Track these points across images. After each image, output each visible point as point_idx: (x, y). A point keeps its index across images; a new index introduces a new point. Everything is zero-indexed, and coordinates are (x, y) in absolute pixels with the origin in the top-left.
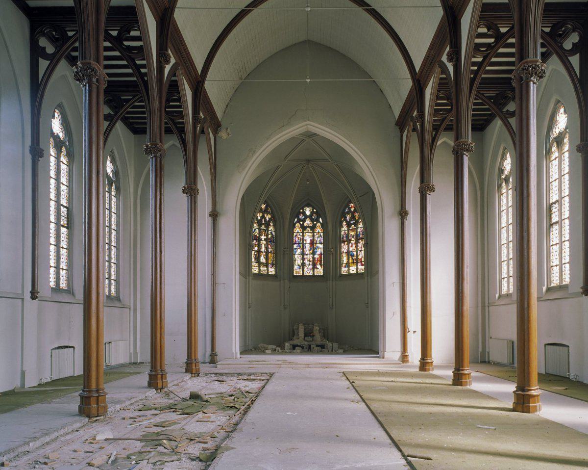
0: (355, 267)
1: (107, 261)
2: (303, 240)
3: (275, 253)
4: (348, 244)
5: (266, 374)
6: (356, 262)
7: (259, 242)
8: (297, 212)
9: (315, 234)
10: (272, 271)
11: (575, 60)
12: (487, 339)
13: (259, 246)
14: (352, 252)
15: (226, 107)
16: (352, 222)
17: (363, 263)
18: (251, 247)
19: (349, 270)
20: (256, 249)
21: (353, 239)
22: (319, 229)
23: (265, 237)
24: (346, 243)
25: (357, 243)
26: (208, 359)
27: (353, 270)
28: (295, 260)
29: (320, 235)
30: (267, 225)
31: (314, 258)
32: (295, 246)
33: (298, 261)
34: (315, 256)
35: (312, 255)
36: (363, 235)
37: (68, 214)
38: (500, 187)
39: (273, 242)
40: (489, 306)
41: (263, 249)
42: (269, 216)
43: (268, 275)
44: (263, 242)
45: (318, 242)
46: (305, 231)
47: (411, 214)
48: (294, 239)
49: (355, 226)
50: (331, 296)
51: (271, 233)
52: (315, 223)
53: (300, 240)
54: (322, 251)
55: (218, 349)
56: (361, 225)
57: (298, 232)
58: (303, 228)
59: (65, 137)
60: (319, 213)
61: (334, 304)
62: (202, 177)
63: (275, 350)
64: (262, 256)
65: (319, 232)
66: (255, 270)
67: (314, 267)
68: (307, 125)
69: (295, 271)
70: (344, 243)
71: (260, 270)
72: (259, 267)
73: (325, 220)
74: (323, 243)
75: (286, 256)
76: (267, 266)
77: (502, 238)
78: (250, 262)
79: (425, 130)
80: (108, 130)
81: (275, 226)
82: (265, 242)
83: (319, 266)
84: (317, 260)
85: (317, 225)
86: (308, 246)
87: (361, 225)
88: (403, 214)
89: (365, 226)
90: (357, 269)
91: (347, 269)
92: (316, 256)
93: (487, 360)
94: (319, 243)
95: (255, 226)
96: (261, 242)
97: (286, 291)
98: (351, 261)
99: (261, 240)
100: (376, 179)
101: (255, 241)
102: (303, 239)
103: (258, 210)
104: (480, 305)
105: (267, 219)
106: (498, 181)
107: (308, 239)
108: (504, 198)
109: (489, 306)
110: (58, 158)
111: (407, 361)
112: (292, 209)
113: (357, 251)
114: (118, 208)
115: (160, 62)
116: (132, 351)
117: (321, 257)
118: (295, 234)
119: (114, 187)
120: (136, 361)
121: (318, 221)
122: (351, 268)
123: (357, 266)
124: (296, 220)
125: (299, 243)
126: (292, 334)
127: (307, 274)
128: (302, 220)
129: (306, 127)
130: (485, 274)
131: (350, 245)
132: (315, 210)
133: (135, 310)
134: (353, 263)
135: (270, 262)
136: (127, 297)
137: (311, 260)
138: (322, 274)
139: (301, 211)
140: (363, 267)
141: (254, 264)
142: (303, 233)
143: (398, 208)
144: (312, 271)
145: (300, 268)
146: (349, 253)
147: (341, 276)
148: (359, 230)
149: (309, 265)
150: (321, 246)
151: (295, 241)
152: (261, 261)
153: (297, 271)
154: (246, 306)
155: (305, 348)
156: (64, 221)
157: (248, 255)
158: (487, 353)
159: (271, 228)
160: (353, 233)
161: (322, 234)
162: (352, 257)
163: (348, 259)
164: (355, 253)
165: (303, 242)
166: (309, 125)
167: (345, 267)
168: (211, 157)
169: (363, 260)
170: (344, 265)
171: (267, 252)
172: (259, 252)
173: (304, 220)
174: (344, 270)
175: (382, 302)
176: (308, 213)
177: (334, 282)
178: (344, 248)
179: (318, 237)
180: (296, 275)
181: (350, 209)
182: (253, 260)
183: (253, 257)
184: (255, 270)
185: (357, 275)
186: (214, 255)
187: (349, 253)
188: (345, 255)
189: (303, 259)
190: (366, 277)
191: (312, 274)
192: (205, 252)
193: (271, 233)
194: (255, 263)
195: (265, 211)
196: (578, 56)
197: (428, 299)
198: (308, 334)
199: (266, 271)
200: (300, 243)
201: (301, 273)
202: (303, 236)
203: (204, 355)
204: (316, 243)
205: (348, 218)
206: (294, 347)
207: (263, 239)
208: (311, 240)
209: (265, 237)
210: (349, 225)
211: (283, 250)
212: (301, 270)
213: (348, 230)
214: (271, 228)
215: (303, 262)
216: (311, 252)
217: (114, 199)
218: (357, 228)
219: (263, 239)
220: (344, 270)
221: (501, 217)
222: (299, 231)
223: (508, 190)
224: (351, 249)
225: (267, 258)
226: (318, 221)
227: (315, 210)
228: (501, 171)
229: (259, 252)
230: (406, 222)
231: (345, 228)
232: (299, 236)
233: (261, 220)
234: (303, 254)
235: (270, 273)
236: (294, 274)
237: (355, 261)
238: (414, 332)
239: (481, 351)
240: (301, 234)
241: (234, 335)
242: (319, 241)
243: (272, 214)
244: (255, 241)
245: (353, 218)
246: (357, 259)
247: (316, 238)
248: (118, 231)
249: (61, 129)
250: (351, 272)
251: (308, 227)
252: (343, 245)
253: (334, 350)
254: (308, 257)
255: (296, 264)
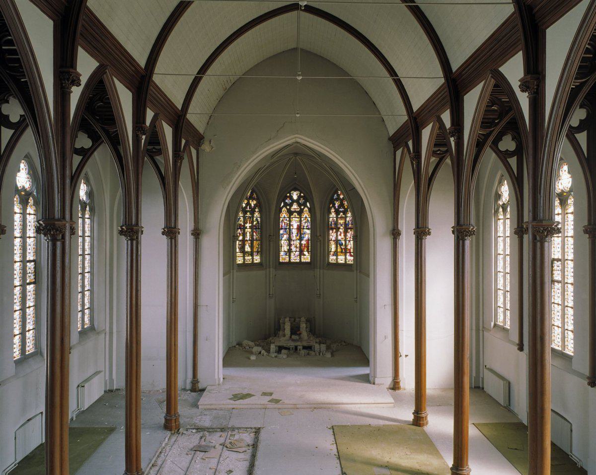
0: (344, 257)
1: (80, 236)
2: (290, 225)
3: (261, 240)
4: (337, 232)
5: (251, 428)
6: (345, 251)
7: (244, 231)
8: (283, 196)
9: (302, 219)
10: (257, 259)
11: (582, 138)
12: (481, 368)
13: (244, 234)
14: (340, 240)
15: (210, 118)
16: (341, 210)
17: (352, 254)
18: (235, 238)
19: (337, 259)
20: (241, 238)
21: (341, 228)
22: (306, 214)
23: (250, 225)
24: (334, 230)
25: (346, 232)
26: (189, 386)
27: (341, 259)
28: (281, 246)
29: (308, 220)
30: (252, 212)
31: (300, 244)
32: (281, 232)
33: (285, 248)
34: (302, 242)
35: (299, 241)
36: (352, 224)
37: (35, 268)
38: (497, 212)
39: (259, 229)
40: (483, 331)
41: (248, 237)
42: (255, 202)
43: (253, 264)
44: (248, 230)
45: (305, 228)
46: (292, 216)
47: (404, 233)
48: (281, 224)
49: (343, 214)
50: (318, 288)
51: (257, 219)
52: (302, 207)
53: (287, 225)
54: (310, 236)
55: (200, 376)
56: (349, 215)
57: (284, 217)
58: (290, 213)
59: (33, 185)
60: (306, 198)
61: (322, 293)
62: (182, 188)
63: (260, 353)
64: (247, 244)
65: (306, 217)
66: (240, 260)
67: (301, 253)
68: (295, 138)
69: (281, 257)
70: (333, 231)
71: (244, 259)
72: (244, 257)
73: (312, 204)
74: (311, 229)
75: (271, 243)
76: (252, 255)
77: (498, 265)
78: (234, 253)
79: (421, 175)
80: (79, 170)
81: (260, 212)
82: (250, 230)
83: (306, 253)
84: (304, 246)
85: (305, 210)
86: (294, 232)
87: (349, 215)
88: (395, 234)
89: (353, 215)
90: (346, 259)
91: (335, 257)
92: (304, 242)
93: (481, 386)
94: (307, 229)
95: (241, 214)
96: (246, 230)
97: (271, 279)
98: (339, 250)
99: (246, 228)
100: (368, 197)
101: (239, 230)
102: (290, 224)
103: (245, 197)
104: (474, 328)
105: (253, 205)
106: (495, 206)
107: (295, 224)
108: (500, 223)
109: (483, 331)
110: (24, 214)
111: (399, 388)
112: (279, 194)
113: (345, 241)
114: (92, 230)
115: (137, 136)
116: (107, 378)
117: (308, 243)
118: (281, 219)
119: (88, 209)
120: (112, 388)
121: (305, 206)
122: (339, 257)
123: (346, 256)
124: (282, 204)
125: (286, 229)
126: (277, 329)
127: (294, 261)
128: (288, 205)
129: (294, 139)
130: (479, 320)
131: (339, 233)
132: (302, 195)
133: (111, 333)
134: (342, 252)
135: (255, 250)
136: (102, 323)
137: (298, 246)
138: (309, 261)
139: (288, 195)
140: (352, 258)
141: (239, 254)
142: (290, 218)
143: (391, 227)
144: (298, 258)
145: (286, 255)
146: (337, 242)
147: (329, 264)
148: (348, 219)
149: (296, 251)
150: (308, 232)
151: (282, 226)
152: (246, 250)
153: (283, 258)
154: (230, 300)
155: (291, 349)
156: (30, 278)
157: (232, 247)
158: (481, 379)
159: (257, 215)
160: (341, 221)
161: (309, 219)
162: (340, 246)
163: (337, 247)
164: (344, 243)
165: (290, 227)
166: (297, 138)
167: (333, 255)
168: (193, 176)
169: (352, 251)
170: (332, 253)
171: (252, 240)
172: (244, 241)
173: (291, 205)
174: (332, 259)
175: (373, 318)
176: (295, 197)
177: (322, 271)
178: (333, 235)
179: (305, 222)
180: (282, 262)
181: (338, 195)
182: (238, 250)
183: (237, 247)
184: (240, 260)
185: (345, 265)
186: (196, 275)
187: (337, 242)
188: (333, 243)
189: (290, 245)
190: (355, 271)
191: (299, 261)
192: (186, 271)
193: (257, 219)
194: (239, 253)
195: (251, 198)
196: (585, 133)
197: (423, 370)
198: (295, 330)
199: (251, 260)
200: (286, 229)
201: (287, 260)
202: (290, 221)
203: (185, 381)
204: (303, 229)
205: (336, 205)
206: (280, 349)
207: (248, 227)
208: (298, 225)
209: (250, 225)
210: (337, 212)
211: (269, 236)
212: (288, 257)
213: (337, 218)
214: (257, 215)
215: (290, 247)
216: (298, 237)
217: (88, 221)
218: (346, 217)
219: (248, 227)
220: (332, 259)
221: (497, 243)
222: (286, 216)
223: (505, 219)
224: (339, 238)
225: (252, 247)
226: (305, 206)
227: (302, 195)
228: (498, 196)
229: (244, 241)
230: (399, 243)
231: (333, 215)
232: (285, 221)
233: (246, 207)
234: (290, 239)
235: (255, 262)
236: (281, 261)
237: (343, 251)
238: (406, 356)
239: (475, 376)
240: (288, 219)
241: (217, 361)
242: (307, 226)
243: (258, 199)
244: (239, 230)
245: (342, 205)
246: (346, 249)
247: (303, 224)
248: (92, 272)
249: (28, 178)
250: (340, 262)
251: (295, 212)
252: (331, 232)
253: (321, 354)
254: (295, 243)
255: (283, 250)
